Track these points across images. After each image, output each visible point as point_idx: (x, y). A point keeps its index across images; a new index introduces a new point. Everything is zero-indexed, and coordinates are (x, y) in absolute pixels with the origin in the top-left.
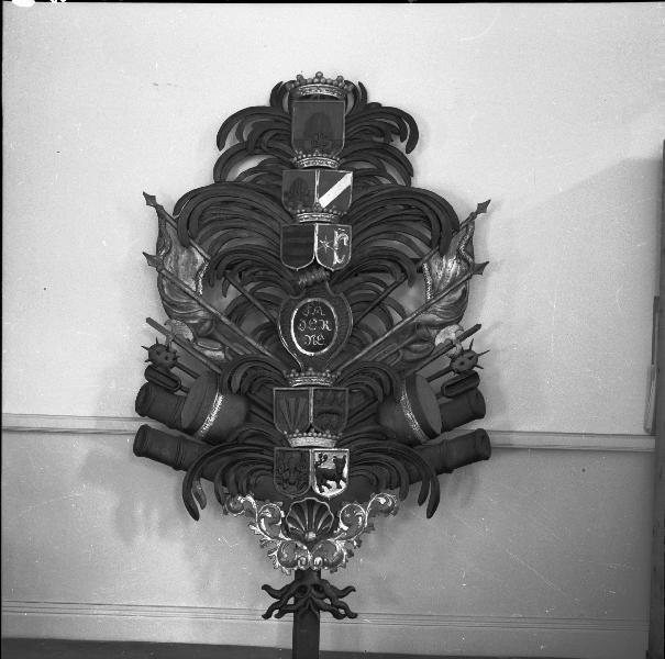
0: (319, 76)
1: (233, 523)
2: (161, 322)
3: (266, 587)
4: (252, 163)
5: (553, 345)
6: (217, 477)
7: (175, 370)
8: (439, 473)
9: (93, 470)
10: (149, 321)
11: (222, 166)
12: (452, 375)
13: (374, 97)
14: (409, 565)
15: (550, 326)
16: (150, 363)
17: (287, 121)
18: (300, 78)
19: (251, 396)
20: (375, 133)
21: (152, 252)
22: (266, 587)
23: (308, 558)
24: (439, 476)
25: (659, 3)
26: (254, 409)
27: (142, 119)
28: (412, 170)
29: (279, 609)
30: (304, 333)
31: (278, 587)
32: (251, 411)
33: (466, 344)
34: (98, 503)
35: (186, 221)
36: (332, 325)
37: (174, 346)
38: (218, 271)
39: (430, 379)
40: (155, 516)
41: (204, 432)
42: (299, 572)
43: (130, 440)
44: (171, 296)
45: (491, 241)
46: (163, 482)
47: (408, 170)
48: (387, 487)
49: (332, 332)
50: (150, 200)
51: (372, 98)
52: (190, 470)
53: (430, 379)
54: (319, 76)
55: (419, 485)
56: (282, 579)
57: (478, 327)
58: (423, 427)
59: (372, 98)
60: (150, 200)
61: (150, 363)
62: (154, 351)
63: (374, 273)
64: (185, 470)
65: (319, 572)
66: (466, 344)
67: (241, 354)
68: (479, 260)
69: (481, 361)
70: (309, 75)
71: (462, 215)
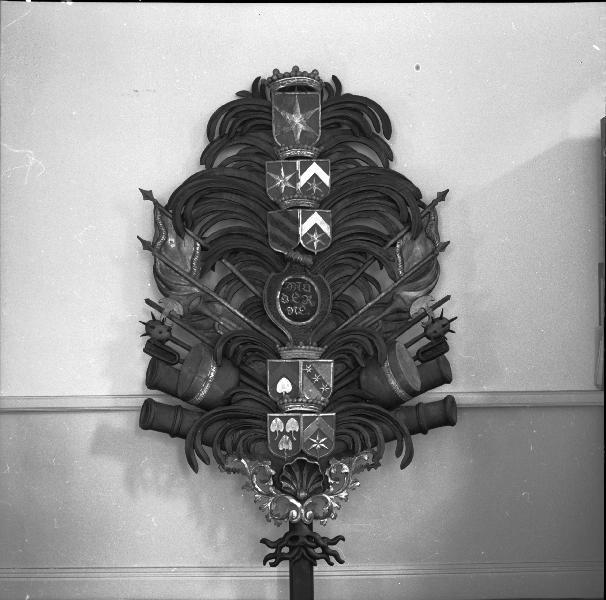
0: (296, 69)
1: (229, 482)
2: (156, 302)
3: (264, 541)
4: (233, 153)
5: (364, 525)
6: (215, 443)
7: (169, 343)
8: (413, 432)
9: (102, 443)
10: (148, 301)
11: (207, 157)
12: (425, 341)
13: (349, 88)
14: (389, 515)
15: (504, 298)
16: (148, 338)
17: (267, 110)
18: (276, 71)
19: (244, 368)
20: (353, 123)
21: (149, 238)
22: (264, 541)
23: (298, 511)
24: (412, 436)
25: (3, 9)
26: (246, 380)
27: (142, 116)
28: (392, 153)
29: (274, 559)
30: (288, 305)
31: (273, 539)
32: (241, 381)
33: (437, 313)
34: (112, 470)
35: (181, 210)
36: (315, 299)
37: (168, 322)
38: (209, 258)
39: (407, 346)
40: (164, 477)
41: (201, 401)
42: (293, 526)
43: (135, 417)
44: (163, 279)
45: (449, 223)
46: (164, 451)
47: (388, 155)
48: (362, 450)
49: (315, 308)
50: (147, 195)
51: (346, 90)
52: (189, 436)
53: (407, 346)
54: (296, 69)
55: (395, 443)
56: (276, 532)
57: (447, 298)
58: (389, 399)
59: (346, 90)
60: (147, 195)
61: (148, 338)
62: (150, 326)
63: (355, 250)
64: (183, 436)
65: (310, 526)
66: (437, 313)
67: (231, 329)
68: (444, 239)
69: (453, 326)
70: (267, 74)
71: (428, 196)
